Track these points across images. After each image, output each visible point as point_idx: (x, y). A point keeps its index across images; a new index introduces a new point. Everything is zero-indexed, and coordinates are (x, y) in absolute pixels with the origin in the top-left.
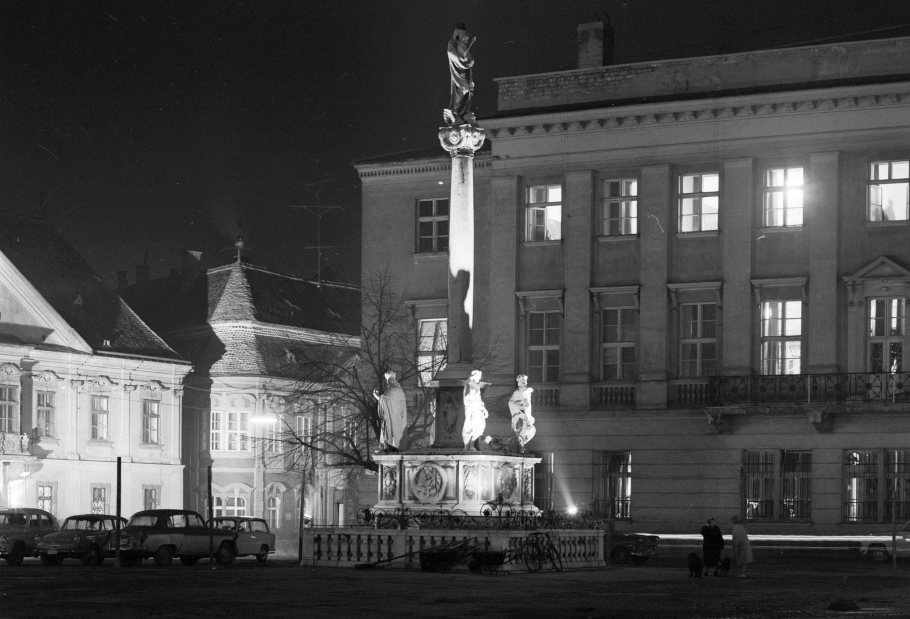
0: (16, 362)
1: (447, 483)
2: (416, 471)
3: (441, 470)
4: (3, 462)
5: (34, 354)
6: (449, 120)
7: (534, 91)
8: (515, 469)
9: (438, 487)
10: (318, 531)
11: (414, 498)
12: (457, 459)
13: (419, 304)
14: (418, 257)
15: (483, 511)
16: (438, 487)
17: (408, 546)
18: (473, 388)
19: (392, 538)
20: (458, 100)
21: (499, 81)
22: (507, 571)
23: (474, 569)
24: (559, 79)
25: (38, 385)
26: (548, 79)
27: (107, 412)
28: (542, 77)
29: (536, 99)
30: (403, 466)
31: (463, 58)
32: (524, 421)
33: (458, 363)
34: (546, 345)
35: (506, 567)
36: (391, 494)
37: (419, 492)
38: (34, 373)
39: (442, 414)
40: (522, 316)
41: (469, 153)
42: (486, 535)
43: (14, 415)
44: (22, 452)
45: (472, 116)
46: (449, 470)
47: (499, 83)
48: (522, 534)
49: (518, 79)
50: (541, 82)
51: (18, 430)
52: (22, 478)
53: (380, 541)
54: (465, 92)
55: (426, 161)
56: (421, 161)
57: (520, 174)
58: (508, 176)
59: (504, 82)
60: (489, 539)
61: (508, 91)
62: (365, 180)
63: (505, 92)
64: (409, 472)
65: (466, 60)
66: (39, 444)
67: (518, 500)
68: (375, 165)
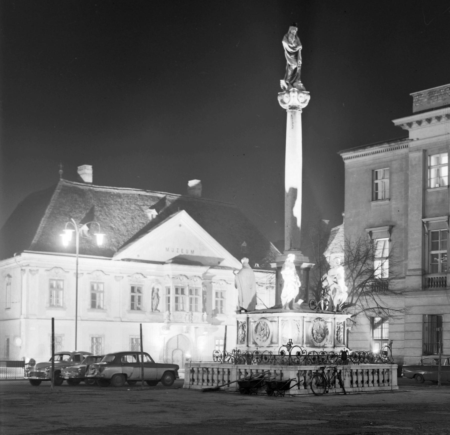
0: (199, 275)
1: (272, 333)
2: (256, 325)
3: (269, 323)
4: (195, 327)
5: (213, 271)
6: (284, 88)
7: (433, 98)
8: (326, 322)
9: (268, 336)
10: (192, 365)
11: (255, 343)
12: (278, 316)
13: (374, 230)
14: (374, 203)
15: (280, 351)
16: (268, 336)
17: (238, 376)
18: (288, 266)
19: (230, 370)
20: (290, 73)
21: (413, 95)
22: (292, 395)
23: (270, 393)
24: (446, 90)
25: (215, 288)
26: (440, 90)
27: (103, 292)
28: (437, 89)
29: (434, 103)
30: (249, 321)
31: (292, 44)
32: (337, 290)
33: (289, 250)
34: (440, 250)
35: (292, 392)
36: (242, 340)
37: (257, 338)
38: (213, 281)
39: (279, 286)
40: (426, 233)
41: (297, 108)
42: (281, 369)
43: (199, 302)
44: (203, 321)
45: (299, 83)
46: (273, 323)
47: (413, 96)
48: (313, 368)
49: (423, 92)
50: (436, 92)
51: (201, 310)
52: (204, 335)
53: (224, 372)
54: (294, 67)
55: (377, 147)
56: (375, 148)
57: (425, 148)
58: (418, 150)
59: (416, 95)
60: (282, 372)
61: (418, 100)
62: (346, 162)
63: (416, 101)
64: (252, 325)
65: (294, 45)
66: (216, 318)
67: (331, 344)
68: (351, 152)
